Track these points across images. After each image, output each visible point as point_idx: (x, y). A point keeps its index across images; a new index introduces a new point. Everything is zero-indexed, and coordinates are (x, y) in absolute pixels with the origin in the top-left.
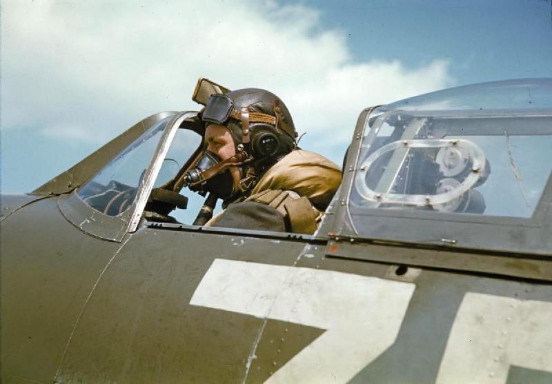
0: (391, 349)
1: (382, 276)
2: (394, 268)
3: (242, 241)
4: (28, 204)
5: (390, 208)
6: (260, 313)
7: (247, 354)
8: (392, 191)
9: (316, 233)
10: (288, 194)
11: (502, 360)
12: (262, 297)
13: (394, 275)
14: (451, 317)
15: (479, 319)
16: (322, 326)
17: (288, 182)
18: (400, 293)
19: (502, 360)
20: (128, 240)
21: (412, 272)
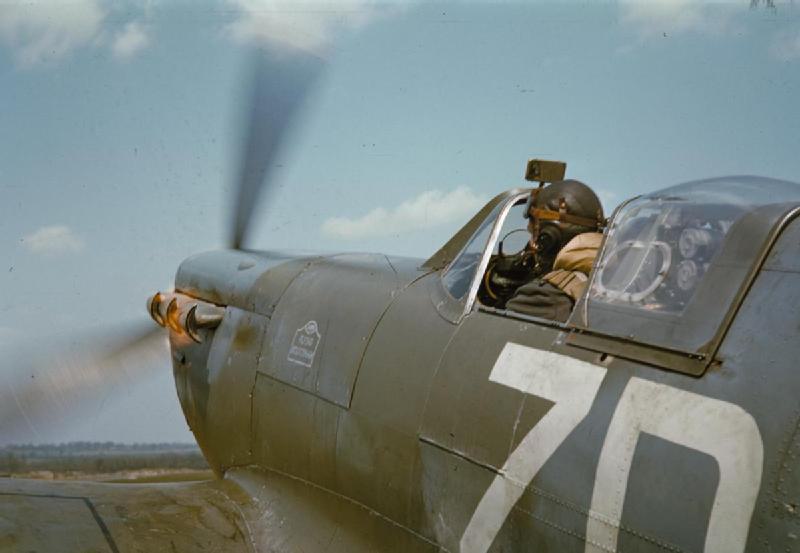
0: (587, 417)
1: (593, 362)
2: (599, 356)
4: (47, 496)
6: (523, 389)
7: (515, 419)
8: (479, 305)
9: (568, 321)
10: (575, 276)
12: (667, 409)
13: (598, 360)
16: (554, 400)
18: (598, 373)
19: (637, 428)
21: (609, 359)
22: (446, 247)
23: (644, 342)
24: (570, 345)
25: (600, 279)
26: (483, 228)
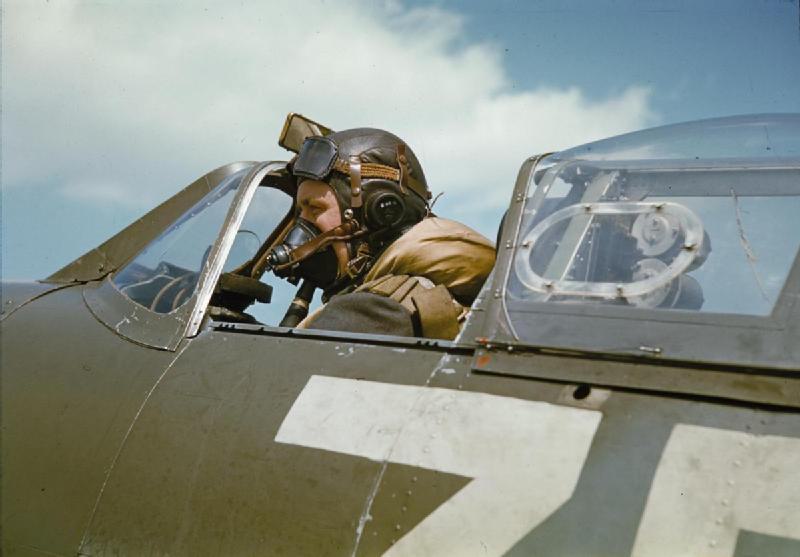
0: (566, 507)
2: (571, 389)
3: (351, 350)
5: (565, 302)
6: (376, 454)
7: (358, 512)
9: (458, 337)
10: (418, 282)
11: (728, 522)
13: (570, 398)
14: (653, 460)
15: (694, 464)
16: (467, 474)
17: (418, 264)
18: (580, 425)
19: (728, 522)
20: (185, 348)
21: (597, 395)
22: (182, 194)
23: (547, 385)
24: (476, 372)
25: (528, 268)
26: (186, 219)
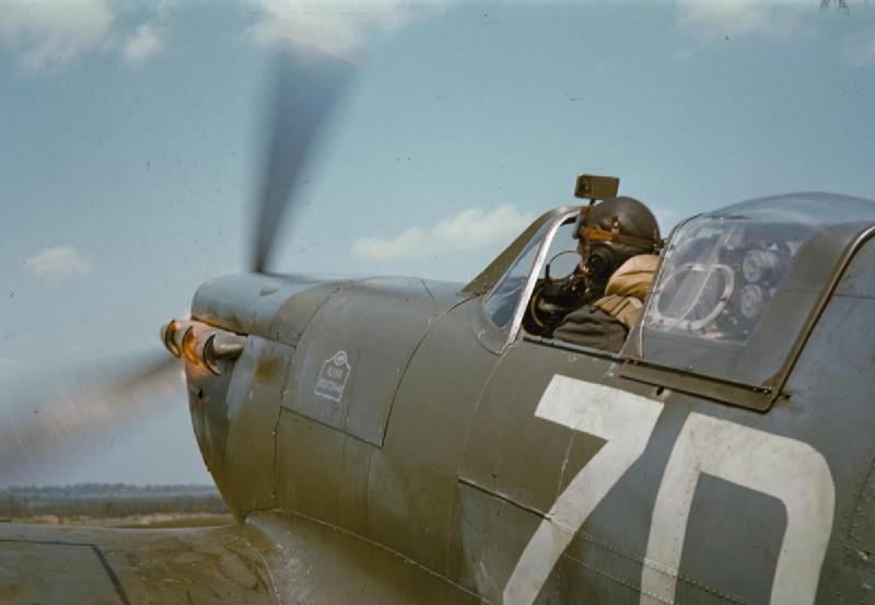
0: (642, 456)
1: (648, 396)
2: (656, 389)
6: (572, 426)
7: (563, 458)
8: (524, 333)
9: (621, 352)
10: (629, 302)
13: (654, 394)
16: (606, 437)
18: (655, 408)
19: (697, 468)
21: (666, 393)
22: (488, 271)
23: (704, 374)
24: (623, 377)
25: (656, 306)
